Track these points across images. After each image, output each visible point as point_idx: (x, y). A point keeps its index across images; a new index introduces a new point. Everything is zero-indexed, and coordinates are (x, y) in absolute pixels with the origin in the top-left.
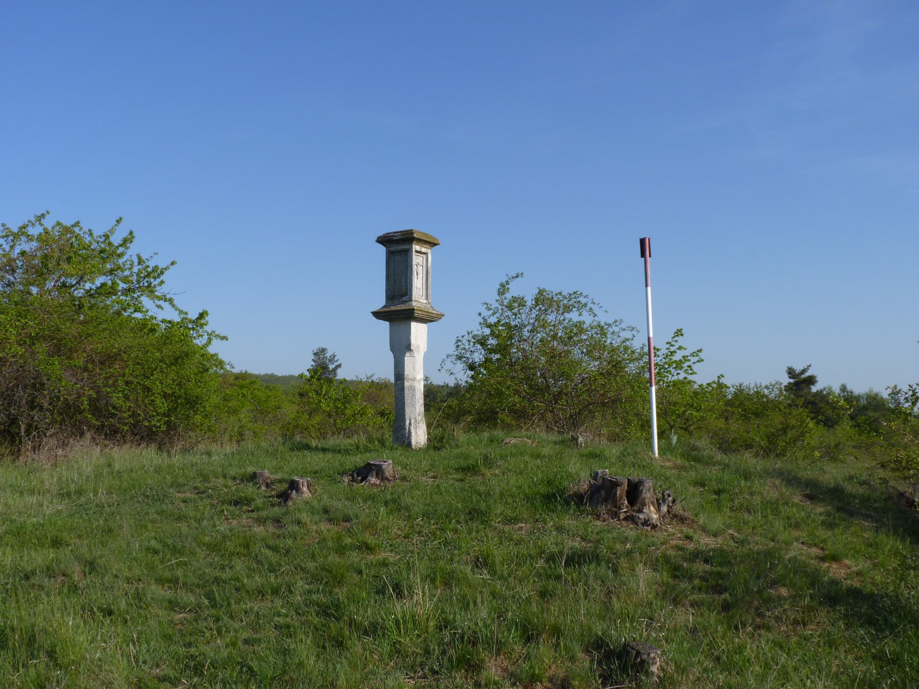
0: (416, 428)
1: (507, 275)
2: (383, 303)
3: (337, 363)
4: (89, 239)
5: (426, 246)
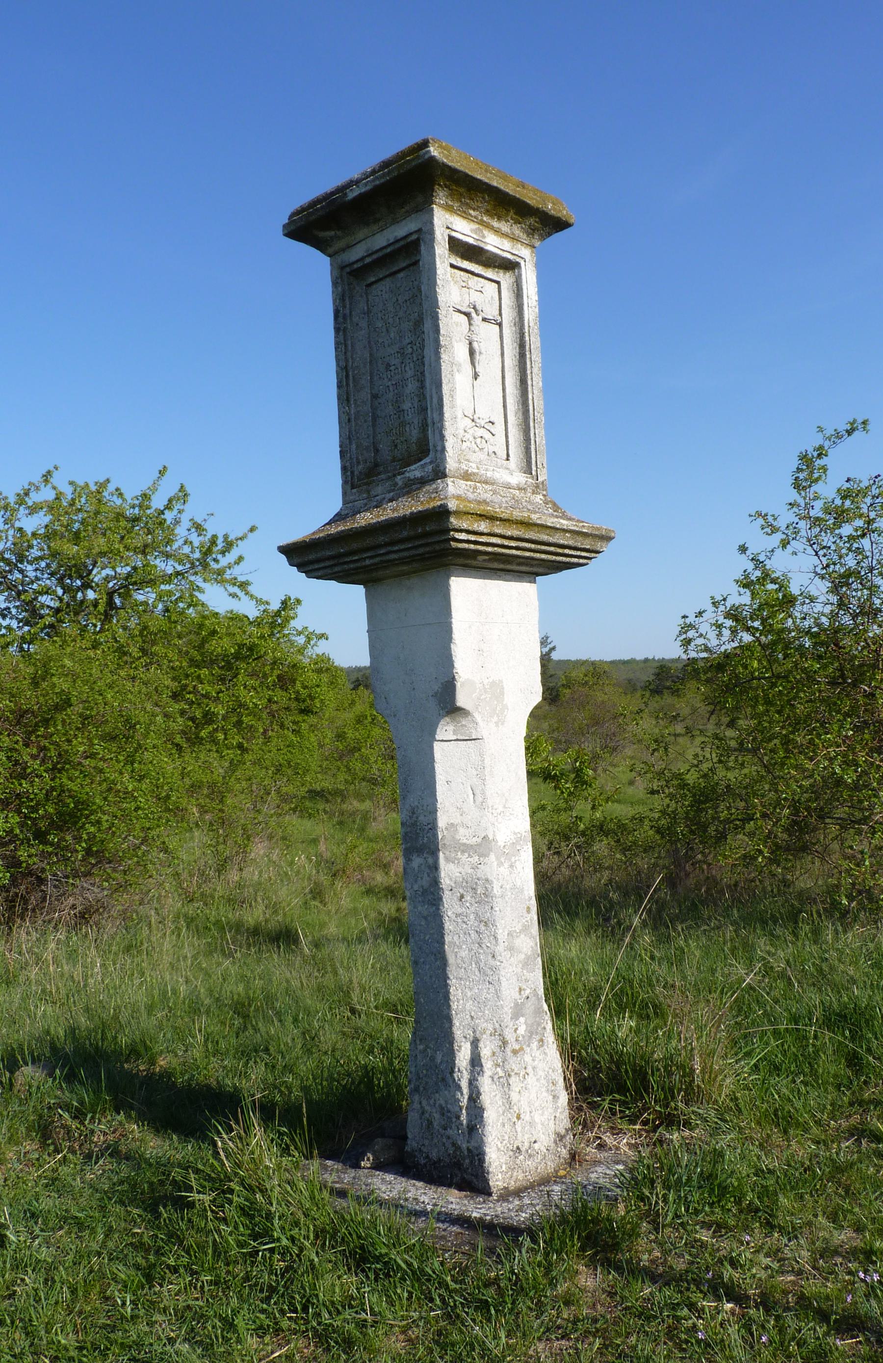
0: (504, 1082)
1: (821, 429)
2: (335, 504)
3: (551, 646)
4: (119, 502)
5: (504, 227)
